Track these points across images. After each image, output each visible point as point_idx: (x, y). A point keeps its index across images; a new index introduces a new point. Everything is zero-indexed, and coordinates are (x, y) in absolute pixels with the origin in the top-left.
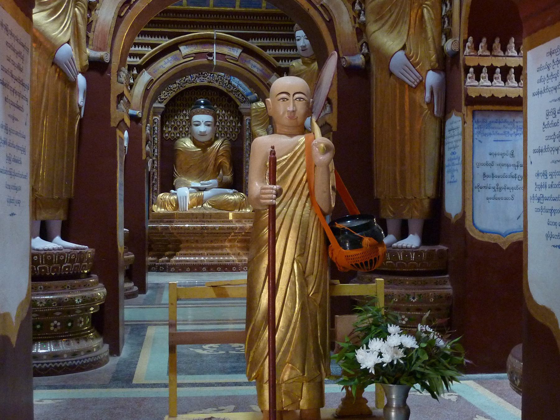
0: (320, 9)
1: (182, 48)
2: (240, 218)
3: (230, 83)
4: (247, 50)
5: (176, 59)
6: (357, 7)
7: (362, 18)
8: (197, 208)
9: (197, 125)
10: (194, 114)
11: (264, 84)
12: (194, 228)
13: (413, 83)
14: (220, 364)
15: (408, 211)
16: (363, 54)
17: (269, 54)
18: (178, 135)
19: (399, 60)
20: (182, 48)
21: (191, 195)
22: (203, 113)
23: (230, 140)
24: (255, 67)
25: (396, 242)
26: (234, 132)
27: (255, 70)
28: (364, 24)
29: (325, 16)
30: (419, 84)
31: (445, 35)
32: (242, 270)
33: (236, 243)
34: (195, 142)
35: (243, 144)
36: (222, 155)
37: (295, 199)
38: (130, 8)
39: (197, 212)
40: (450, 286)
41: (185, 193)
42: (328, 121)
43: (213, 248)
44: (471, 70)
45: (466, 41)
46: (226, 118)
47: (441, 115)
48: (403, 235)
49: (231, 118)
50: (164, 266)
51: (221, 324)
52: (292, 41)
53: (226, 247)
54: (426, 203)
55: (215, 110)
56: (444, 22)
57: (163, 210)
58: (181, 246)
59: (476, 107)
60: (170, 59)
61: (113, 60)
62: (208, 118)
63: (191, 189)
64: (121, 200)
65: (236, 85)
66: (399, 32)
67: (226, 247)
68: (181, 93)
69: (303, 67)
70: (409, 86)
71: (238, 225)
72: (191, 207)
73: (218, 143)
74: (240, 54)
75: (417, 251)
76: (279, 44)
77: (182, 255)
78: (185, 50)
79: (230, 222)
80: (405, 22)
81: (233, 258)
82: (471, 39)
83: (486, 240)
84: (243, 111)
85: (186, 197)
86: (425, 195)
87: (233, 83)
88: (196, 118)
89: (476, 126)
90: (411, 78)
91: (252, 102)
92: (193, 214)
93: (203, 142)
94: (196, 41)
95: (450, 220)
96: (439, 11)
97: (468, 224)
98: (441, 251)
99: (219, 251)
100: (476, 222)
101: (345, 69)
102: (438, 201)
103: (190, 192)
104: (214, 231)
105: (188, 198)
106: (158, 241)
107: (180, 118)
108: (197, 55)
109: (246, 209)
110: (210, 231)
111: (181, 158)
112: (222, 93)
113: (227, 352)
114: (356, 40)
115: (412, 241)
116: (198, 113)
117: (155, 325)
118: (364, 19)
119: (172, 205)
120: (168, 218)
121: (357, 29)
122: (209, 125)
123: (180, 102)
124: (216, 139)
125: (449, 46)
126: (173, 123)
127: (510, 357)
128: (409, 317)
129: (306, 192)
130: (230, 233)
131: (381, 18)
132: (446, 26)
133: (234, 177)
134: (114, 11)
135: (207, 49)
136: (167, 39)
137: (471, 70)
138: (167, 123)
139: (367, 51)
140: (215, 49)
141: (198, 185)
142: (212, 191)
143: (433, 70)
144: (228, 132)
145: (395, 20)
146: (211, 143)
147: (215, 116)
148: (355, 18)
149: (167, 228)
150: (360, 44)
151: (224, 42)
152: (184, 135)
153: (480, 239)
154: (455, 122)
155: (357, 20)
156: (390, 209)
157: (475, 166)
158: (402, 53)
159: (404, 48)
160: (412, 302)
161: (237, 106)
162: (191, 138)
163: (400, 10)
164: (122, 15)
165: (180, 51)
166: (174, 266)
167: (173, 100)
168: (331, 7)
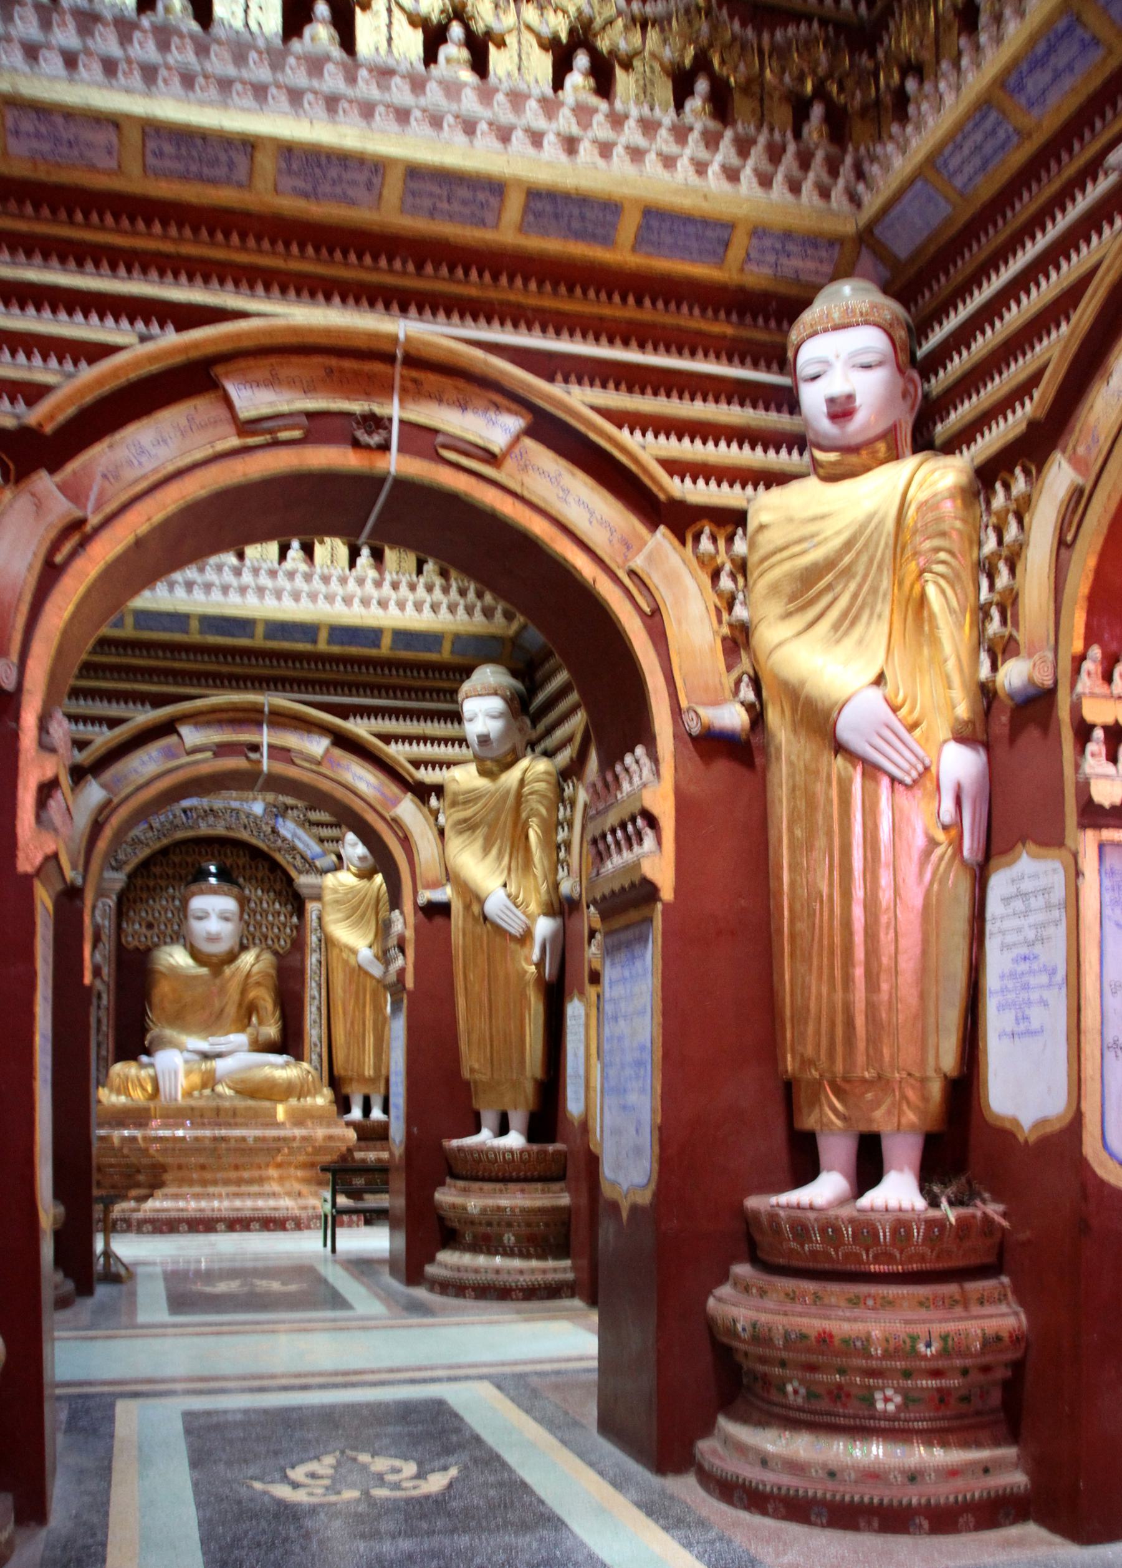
1: (185, 731)
2: (299, 1118)
3: (274, 831)
5: (170, 754)
7: (740, 612)
9: (200, 918)
10: (194, 894)
12: (197, 1139)
13: (908, 774)
14: (362, 1546)
15: (889, 1112)
16: (742, 703)
17: (397, 752)
20: (185, 731)
22: (214, 891)
23: (276, 953)
24: (361, 778)
26: (282, 936)
30: (920, 775)
32: (308, 1227)
34: (195, 954)
36: (258, 984)
39: (202, 1103)
41: (176, 1062)
43: (239, 1182)
44: (1099, 734)
46: (265, 905)
48: (868, 1169)
49: (277, 906)
52: (456, 725)
53: (269, 1179)
54: (936, 1089)
55: (241, 888)
57: (123, 1099)
60: (154, 754)
61: (28, 684)
62: (227, 904)
64: (397, 1118)
65: (289, 836)
66: (860, 642)
67: (269, 1179)
68: (164, 852)
69: (483, 783)
71: (298, 1132)
72: (188, 1094)
73: (248, 959)
77: (166, 1197)
78: (191, 735)
80: (880, 616)
82: (1096, 652)
84: (304, 892)
85: (176, 1073)
86: (938, 1070)
87: (283, 832)
88: (198, 903)
89: (1107, 883)
91: (324, 872)
94: (218, 716)
95: (1014, 1136)
96: (971, 588)
97: (1091, 1148)
98: (557, 1153)
99: (255, 1189)
101: (696, 740)
102: (965, 1086)
103: (186, 1062)
104: (243, 1146)
106: (111, 1166)
107: (161, 906)
108: (222, 750)
109: (314, 1096)
110: (233, 1144)
111: (163, 990)
112: (256, 854)
113: (366, 1493)
114: (722, 665)
116: (202, 893)
117: (136, 1395)
119: (144, 1089)
120: (137, 1117)
121: (724, 639)
122: (227, 919)
124: (243, 948)
125: (1014, 675)
126: (143, 914)
128: (905, 1393)
130: (279, 1150)
131: (802, 609)
133: (285, 1031)
134: (33, 548)
135: (246, 736)
136: (148, 707)
137: (1099, 734)
138: (131, 914)
140: (266, 737)
141: (203, 1045)
142: (238, 1056)
144: (270, 934)
145: (845, 615)
146: (231, 957)
147: (243, 902)
148: (718, 611)
149: (133, 1139)
150: (735, 674)
151: (287, 721)
152: (168, 940)
155: (725, 616)
157: (1107, 989)
158: (876, 694)
161: (290, 881)
162: (185, 946)
163: (860, 587)
164: (59, 558)
165: (180, 736)
167: (145, 865)
168: (655, 579)
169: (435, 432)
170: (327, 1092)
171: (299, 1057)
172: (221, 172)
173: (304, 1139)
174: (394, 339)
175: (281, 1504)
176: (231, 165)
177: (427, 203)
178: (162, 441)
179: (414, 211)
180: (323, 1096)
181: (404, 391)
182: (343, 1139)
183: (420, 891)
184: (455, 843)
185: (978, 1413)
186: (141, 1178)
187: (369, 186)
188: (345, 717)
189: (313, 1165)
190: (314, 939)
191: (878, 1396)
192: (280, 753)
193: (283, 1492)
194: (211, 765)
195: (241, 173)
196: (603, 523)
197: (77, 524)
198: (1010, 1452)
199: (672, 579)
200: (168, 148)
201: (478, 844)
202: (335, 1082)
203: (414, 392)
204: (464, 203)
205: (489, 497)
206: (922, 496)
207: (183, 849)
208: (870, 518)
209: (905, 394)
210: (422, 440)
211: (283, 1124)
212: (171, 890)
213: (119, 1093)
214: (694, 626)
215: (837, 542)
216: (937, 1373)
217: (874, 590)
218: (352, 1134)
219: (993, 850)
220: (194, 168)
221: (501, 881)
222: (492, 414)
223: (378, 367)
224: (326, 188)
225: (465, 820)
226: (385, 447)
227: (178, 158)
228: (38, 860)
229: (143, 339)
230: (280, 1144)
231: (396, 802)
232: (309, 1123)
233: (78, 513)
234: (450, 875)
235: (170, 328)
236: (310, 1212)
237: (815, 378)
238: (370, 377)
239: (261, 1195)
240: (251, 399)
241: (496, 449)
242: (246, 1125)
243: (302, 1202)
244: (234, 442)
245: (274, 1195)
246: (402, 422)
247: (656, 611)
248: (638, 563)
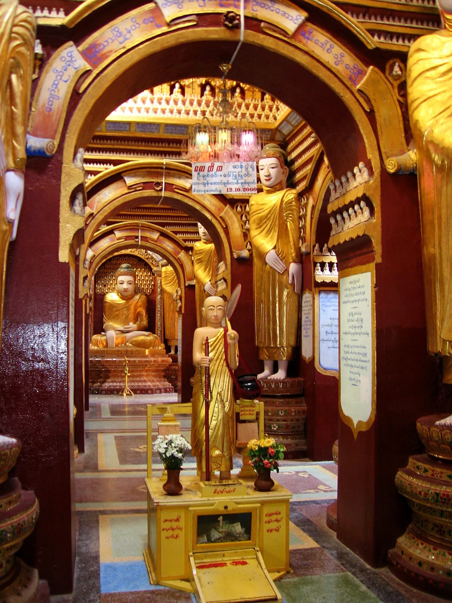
0: (220, 219)
2: (153, 354)
4: (163, 234)
5: (112, 240)
6: (244, 218)
7: (247, 226)
8: (121, 347)
11: (175, 258)
17: (179, 237)
18: (107, 291)
19: (271, 257)
21: (117, 336)
23: (146, 295)
25: (269, 376)
27: (169, 249)
28: (248, 230)
29: (223, 224)
30: (284, 271)
31: (302, 240)
32: (156, 393)
33: (151, 373)
35: (156, 297)
36: (140, 306)
37: (218, 361)
38: (92, 219)
39: (122, 349)
40: (305, 405)
42: (225, 294)
45: (314, 246)
46: (143, 278)
47: (299, 292)
48: (275, 370)
50: (98, 390)
51: (141, 432)
53: (143, 375)
56: (301, 232)
57: (96, 347)
58: (110, 375)
59: (321, 288)
63: (117, 332)
66: (271, 237)
67: (143, 375)
70: (278, 272)
71: (152, 359)
74: (158, 237)
75: (283, 382)
76: (186, 230)
78: (118, 234)
79: (147, 357)
81: (149, 384)
82: (317, 245)
83: (328, 374)
85: (113, 338)
90: (279, 267)
92: (118, 351)
93: (126, 296)
96: (297, 224)
99: (138, 379)
100: (321, 363)
102: (297, 349)
103: (116, 334)
105: (115, 339)
108: (127, 238)
115: (281, 375)
117: (102, 433)
118: (249, 227)
119: (103, 344)
122: (130, 284)
123: (108, 266)
126: (103, 282)
127: (334, 446)
129: (224, 357)
130: (146, 365)
131: (260, 227)
132: (302, 234)
137: (319, 264)
138: (99, 282)
139: (250, 248)
143: (294, 262)
146: (132, 297)
148: (242, 226)
153: (324, 374)
154: (307, 296)
155: (244, 227)
156: (266, 354)
157: (321, 326)
159: (275, 248)
160: (281, 416)
164: (88, 223)
166: (105, 390)
168: (227, 218)
169: (173, 185)
170: (163, 345)
171: (154, 333)
172: (123, 129)
173: (155, 361)
174: (162, 164)
175: (137, 452)
176: (125, 127)
177: (170, 131)
178: (110, 193)
179: (167, 133)
180: (161, 347)
181: (166, 175)
182: (167, 361)
183: (186, 282)
184: (196, 266)
185: (297, 431)
186: (102, 375)
187: (157, 129)
188: (164, 227)
189: (157, 371)
190: (159, 290)
191: (272, 426)
192: (144, 238)
193: (138, 450)
194: (123, 242)
195: (128, 129)
196: (214, 205)
197: (92, 214)
198: (303, 441)
199: (231, 218)
200: (112, 125)
201: (203, 267)
202: (166, 341)
203: (168, 175)
204: (179, 130)
205: (186, 200)
206: (286, 200)
207: (116, 258)
208: (275, 205)
209: (283, 173)
210: (169, 187)
211: (147, 355)
212: (112, 273)
213: (95, 346)
214: (236, 230)
215: (267, 211)
216: (285, 421)
217: (275, 224)
218: (170, 360)
219: (302, 291)
220: (117, 129)
221: (209, 279)
222: (187, 180)
223: (160, 170)
224: (146, 130)
225: (199, 259)
226: (161, 190)
227: (114, 127)
228: (83, 295)
229: (106, 169)
230: (147, 363)
231: (179, 253)
232: (156, 356)
233: (92, 212)
234: (195, 277)
235: (112, 165)
236: (157, 387)
237: (262, 169)
238: (158, 172)
239: (141, 381)
240: (130, 181)
241: (187, 188)
242: (136, 357)
243: (154, 384)
244: (127, 191)
245: (145, 381)
246: (165, 183)
247: (227, 227)
248: (222, 214)
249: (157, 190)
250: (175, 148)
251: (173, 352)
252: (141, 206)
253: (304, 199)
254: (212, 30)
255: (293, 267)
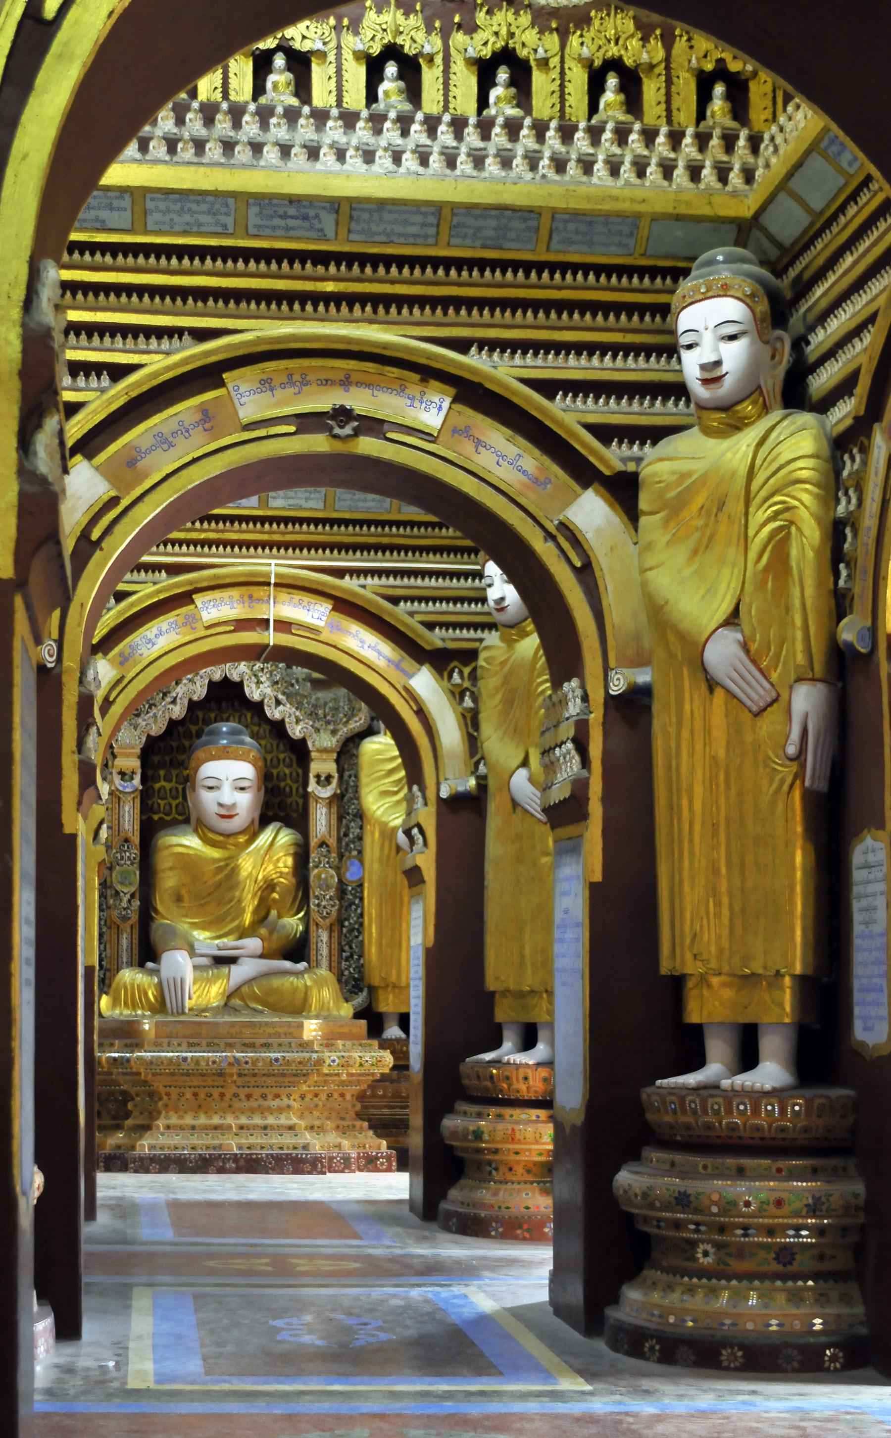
48: (748, 1058)
79: (306, 1046)
115: (771, 1073)
159: (733, 619)
218: (388, 1058)
237: (690, 347)
249: (336, 437)
250: (371, 281)
251: (393, 1031)
252: (217, 511)
253: (853, 459)
254: (793, 938)
255: (806, 701)
